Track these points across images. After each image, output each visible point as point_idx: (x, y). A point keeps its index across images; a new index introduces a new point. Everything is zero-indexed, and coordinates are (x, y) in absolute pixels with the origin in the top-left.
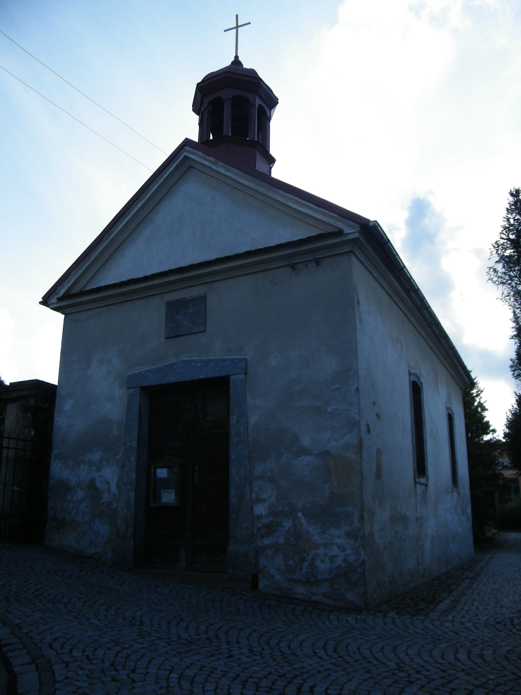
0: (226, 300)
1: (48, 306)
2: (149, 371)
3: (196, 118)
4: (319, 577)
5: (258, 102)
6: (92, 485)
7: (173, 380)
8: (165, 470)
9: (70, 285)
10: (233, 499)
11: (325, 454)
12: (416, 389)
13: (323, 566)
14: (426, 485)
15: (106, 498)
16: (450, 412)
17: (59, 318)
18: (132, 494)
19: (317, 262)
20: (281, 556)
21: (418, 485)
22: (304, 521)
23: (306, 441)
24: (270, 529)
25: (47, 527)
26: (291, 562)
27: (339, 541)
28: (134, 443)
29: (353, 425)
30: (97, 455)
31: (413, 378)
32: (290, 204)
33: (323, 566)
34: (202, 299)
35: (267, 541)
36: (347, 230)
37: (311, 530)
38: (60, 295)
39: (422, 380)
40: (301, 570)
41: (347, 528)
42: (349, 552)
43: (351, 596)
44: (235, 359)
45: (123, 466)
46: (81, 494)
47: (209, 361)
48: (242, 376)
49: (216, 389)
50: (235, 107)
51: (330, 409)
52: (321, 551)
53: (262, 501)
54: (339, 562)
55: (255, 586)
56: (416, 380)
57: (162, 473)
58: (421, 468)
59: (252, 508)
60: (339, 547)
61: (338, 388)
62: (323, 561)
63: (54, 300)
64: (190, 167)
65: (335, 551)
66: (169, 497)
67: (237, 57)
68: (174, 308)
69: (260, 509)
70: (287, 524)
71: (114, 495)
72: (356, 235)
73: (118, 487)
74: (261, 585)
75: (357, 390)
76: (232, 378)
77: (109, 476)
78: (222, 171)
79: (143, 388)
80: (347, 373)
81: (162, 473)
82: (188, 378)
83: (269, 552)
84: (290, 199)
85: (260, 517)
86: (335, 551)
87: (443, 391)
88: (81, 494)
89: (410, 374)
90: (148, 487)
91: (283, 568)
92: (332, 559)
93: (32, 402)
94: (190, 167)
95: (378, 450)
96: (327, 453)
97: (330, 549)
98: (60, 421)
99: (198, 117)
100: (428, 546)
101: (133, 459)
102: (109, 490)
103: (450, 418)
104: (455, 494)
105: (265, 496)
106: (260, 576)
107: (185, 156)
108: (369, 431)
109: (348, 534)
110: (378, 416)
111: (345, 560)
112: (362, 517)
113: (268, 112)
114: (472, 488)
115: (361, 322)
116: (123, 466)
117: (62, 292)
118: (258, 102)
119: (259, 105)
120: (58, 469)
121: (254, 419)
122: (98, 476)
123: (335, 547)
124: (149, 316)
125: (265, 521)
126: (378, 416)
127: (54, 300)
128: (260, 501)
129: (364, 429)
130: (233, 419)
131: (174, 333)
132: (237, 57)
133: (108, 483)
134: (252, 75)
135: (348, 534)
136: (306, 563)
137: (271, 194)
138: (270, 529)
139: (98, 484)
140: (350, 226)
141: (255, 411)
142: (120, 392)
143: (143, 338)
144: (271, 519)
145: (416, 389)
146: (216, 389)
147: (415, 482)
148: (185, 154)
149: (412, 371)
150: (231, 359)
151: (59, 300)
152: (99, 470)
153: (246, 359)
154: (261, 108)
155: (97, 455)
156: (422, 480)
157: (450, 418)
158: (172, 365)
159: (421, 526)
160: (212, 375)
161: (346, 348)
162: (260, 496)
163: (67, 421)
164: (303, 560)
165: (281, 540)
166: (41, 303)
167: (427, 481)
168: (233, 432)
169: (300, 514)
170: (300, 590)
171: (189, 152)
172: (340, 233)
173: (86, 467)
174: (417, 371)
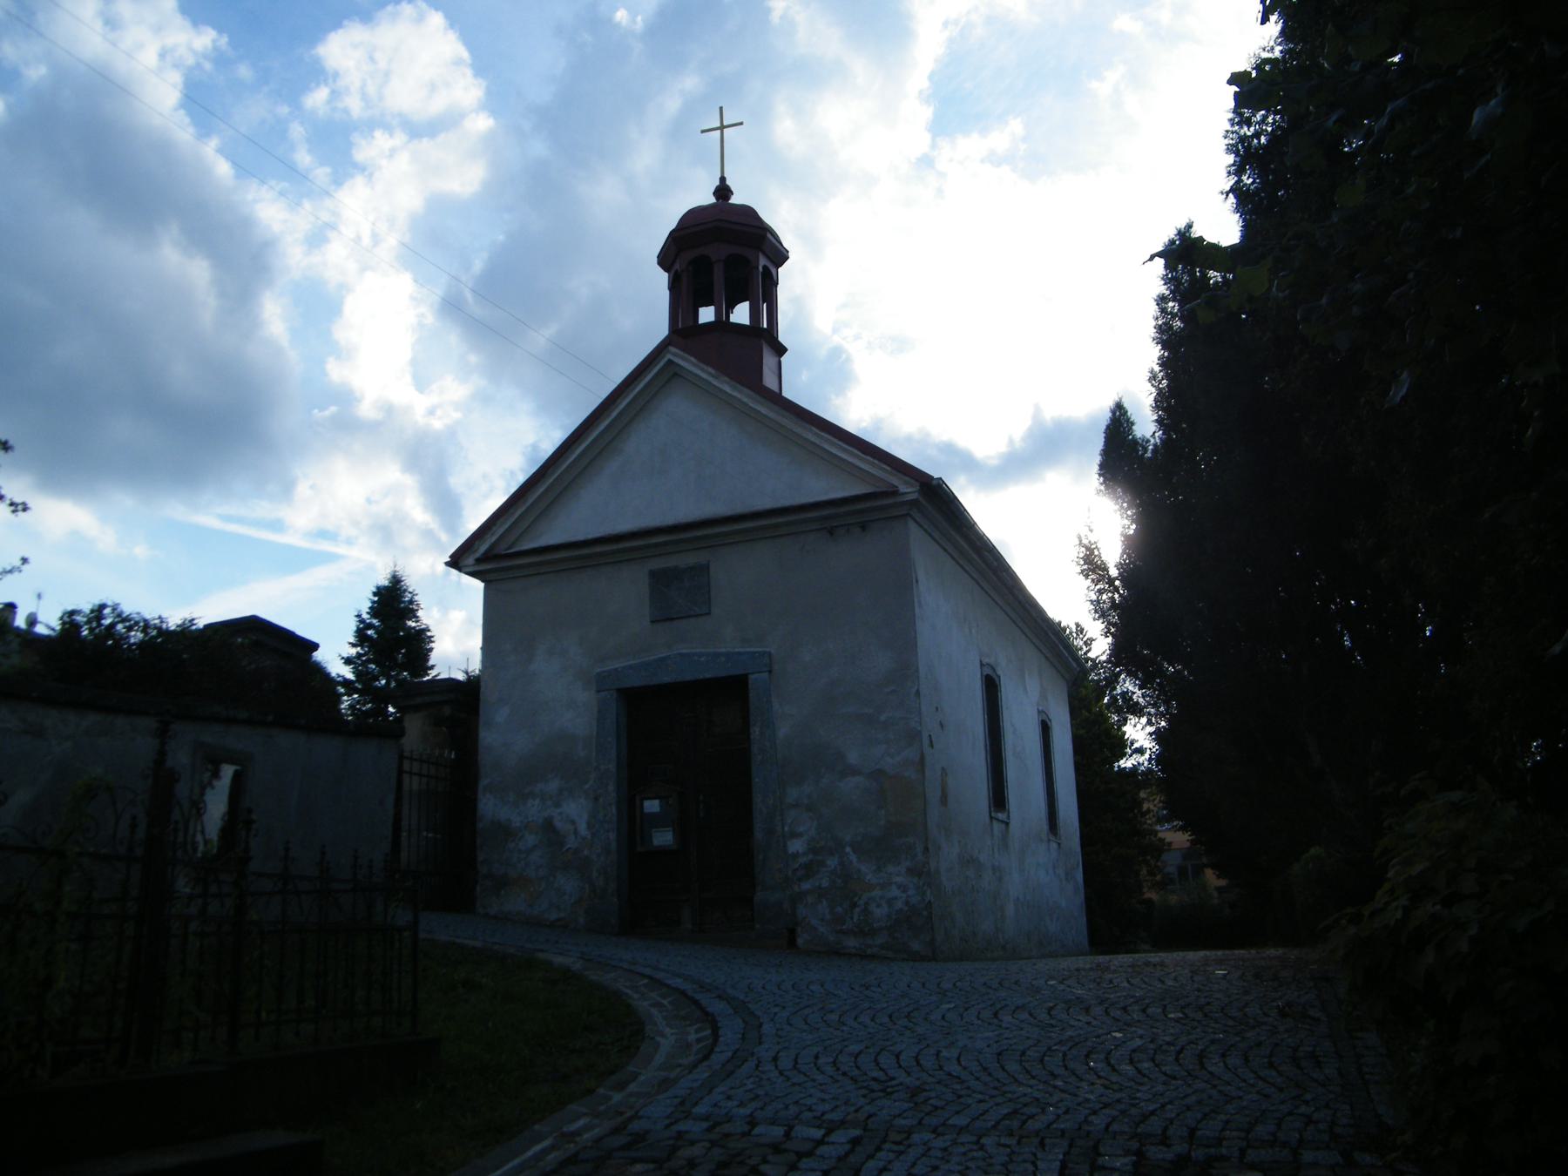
0: (737, 573)
1: (460, 569)
2: (630, 667)
3: (663, 278)
5: (763, 261)
6: (548, 826)
7: (666, 679)
8: (656, 802)
9: (494, 539)
10: (759, 834)
12: (991, 687)
13: (880, 912)
15: (571, 843)
17: (477, 586)
18: (612, 836)
19: (864, 527)
21: (995, 824)
22: (854, 858)
23: (853, 757)
24: (809, 870)
25: (478, 889)
26: (839, 909)
27: (898, 879)
28: (612, 767)
29: (914, 736)
30: (554, 785)
31: (988, 671)
32: (826, 447)
33: (880, 912)
34: (704, 569)
35: (806, 886)
36: (903, 489)
37: (863, 868)
38: (477, 555)
42: (911, 892)
43: (916, 946)
45: (596, 799)
46: (531, 839)
47: (718, 655)
48: (766, 675)
49: (730, 692)
50: (724, 256)
51: (883, 718)
52: (877, 893)
53: (800, 835)
54: (899, 905)
55: (792, 943)
57: (652, 806)
58: (999, 799)
59: (785, 846)
60: (899, 887)
62: (878, 906)
63: (470, 560)
64: (676, 374)
65: (895, 892)
66: (663, 838)
67: (723, 179)
68: (660, 580)
69: (796, 846)
70: (832, 862)
71: (584, 839)
72: (914, 496)
73: (590, 826)
74: (800, 941)
75: (918, 693)
76: (751, 677)
77: (575, 814)
78: (727, 389)
79: (619, 691)
80: (905, 671)
81: (652, 806)
82: (688, 677)
84: (827, 440)
85: (795, 856)
86: (895, 892)
87: (1033, 686)
88: (531, 839)
89: (982, 665)
90: (633, 826)
91: (828, 917)
92: (890, 902)
93: (447, 711)
94: (676, 374)
97: (888, 890)
98: (489, 737)
99: (666, 275)
100: (1010, 910)
101: (611, 788)
102: (576, 832)
103: (1045, 728)
104: (1054, 845)
105: (801, 829)
107: (670, 362)
108: (931, 745)
109: (910, 871)
110: (942, 725)
111: (907, 903)
112: (926, 849)
113: (773, 271)
114: (1086, 840)
115: (920, 606)
116: (596, 799)
117: (483, 548)
119: (765, 267)
120: (489, 806)
121: (783, 730)
122: (555, 810)
123: (894, 887)
124: (626, 591)
125: (803, 860)
126: (942, 725)
127: (470, 560)
128: (795, 835)
129: (926, 742)
130: (756, 731)
131: (663, 616)
132: (723, 179)
133: (573, 822)
134: (749, 213)
135: (910, 871)
136: (857, 910)
137: (798, 430)
138: (809, 870)
139: (558, 824)
140: (906, 483)
141: (785, 719)
142: (585, 697)
143: (620, 624)
145: (991, 687)
146: (730, 692)
148: (669, 356)
149: (986, 661)
151: (478, 561)
152: (557, 805)
153: (770, 654)
154: (766, 270)
155: (554, 785)
156: (1000, 816)
157: (1045, 728)
158: (662, 660)
159: (1000, 879)
160: (723, 673)
161: (903, 641)
162: (793, 828)
163: (501, 736)
164: (854, 905)
165: (825, 883)
166: (447, 564)
168: (755, 749)
169: (848, 849)
170: (852, 943)
171: (675, 355)
172: (895, 493)
173: (537, 802)
174: (991, 660)
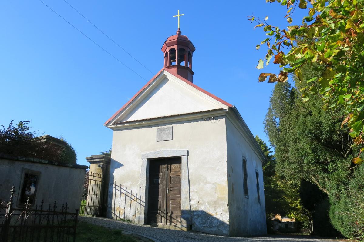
4: (213, 225)
11: (215, 184)
12: (244, 162)
14: (248, 199)
16: (257, 171)
20: (200, 218)
23: (209, 179)
39: (247, 159)
40: (207, 223)
41: (223, 209)
44: (183, 150)
51: (217, 169)
56: (244, 158)
58: (246, 192)
61: (220, 161)
79: (148, 159)
83: (196, 217)
89: (242, 156)
95: (233, 183)
96: (216, 183)
103: (257, 174)
106: (193, 225)
118: (189, 50)
136: (209, 221)
144: (197, 205)
145: (244, 162)
147: (244, 197)
150: (182, 150)
156: (246, 196)
157: (257, 174)
164: (208, 219)
167: (248, 197)
